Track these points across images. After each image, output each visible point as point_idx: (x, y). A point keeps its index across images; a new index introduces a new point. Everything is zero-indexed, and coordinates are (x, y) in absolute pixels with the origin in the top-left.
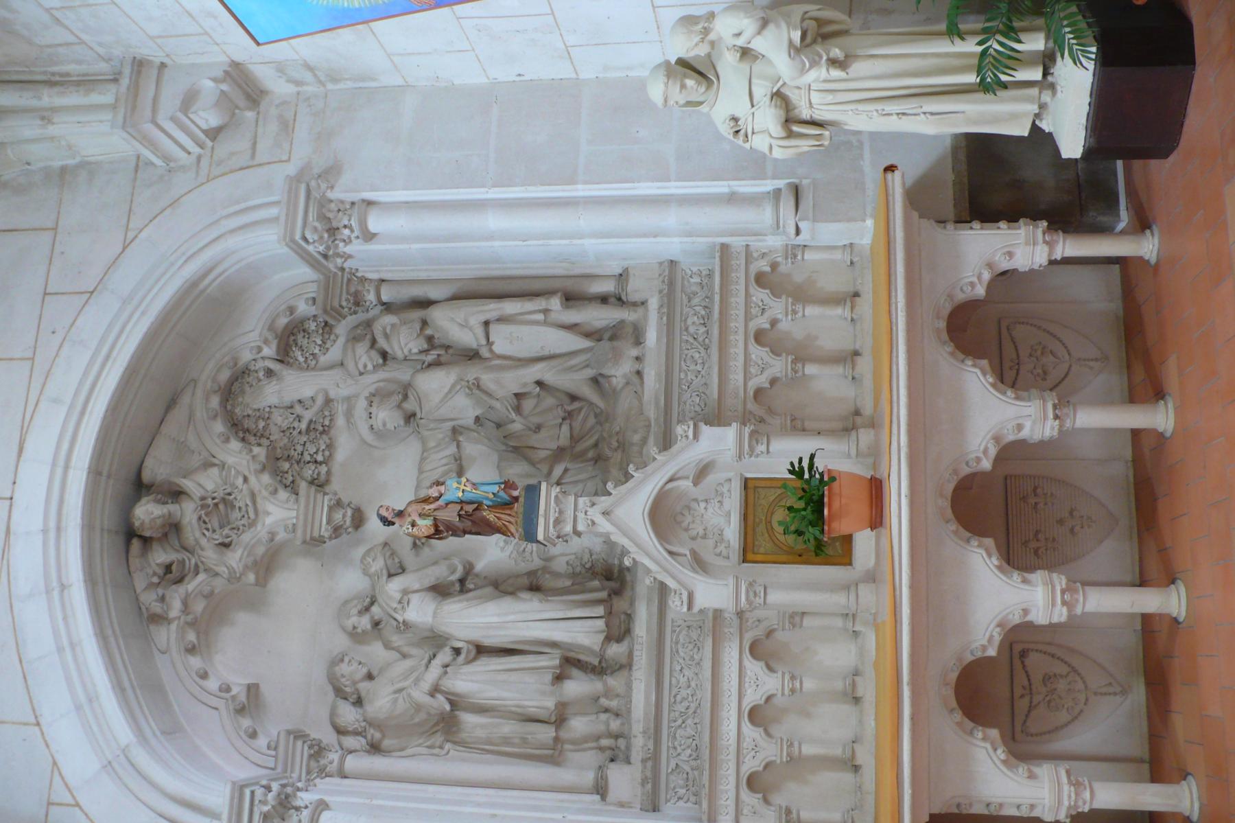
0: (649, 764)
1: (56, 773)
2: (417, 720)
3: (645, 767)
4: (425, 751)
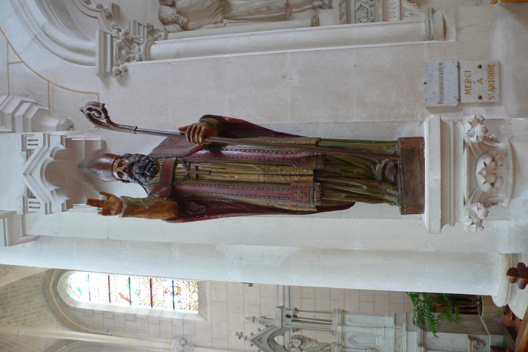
0: (344, 5)
1: (9, 47)
2: (206, 6)
3: (341, 8)
4: (213, 25)
